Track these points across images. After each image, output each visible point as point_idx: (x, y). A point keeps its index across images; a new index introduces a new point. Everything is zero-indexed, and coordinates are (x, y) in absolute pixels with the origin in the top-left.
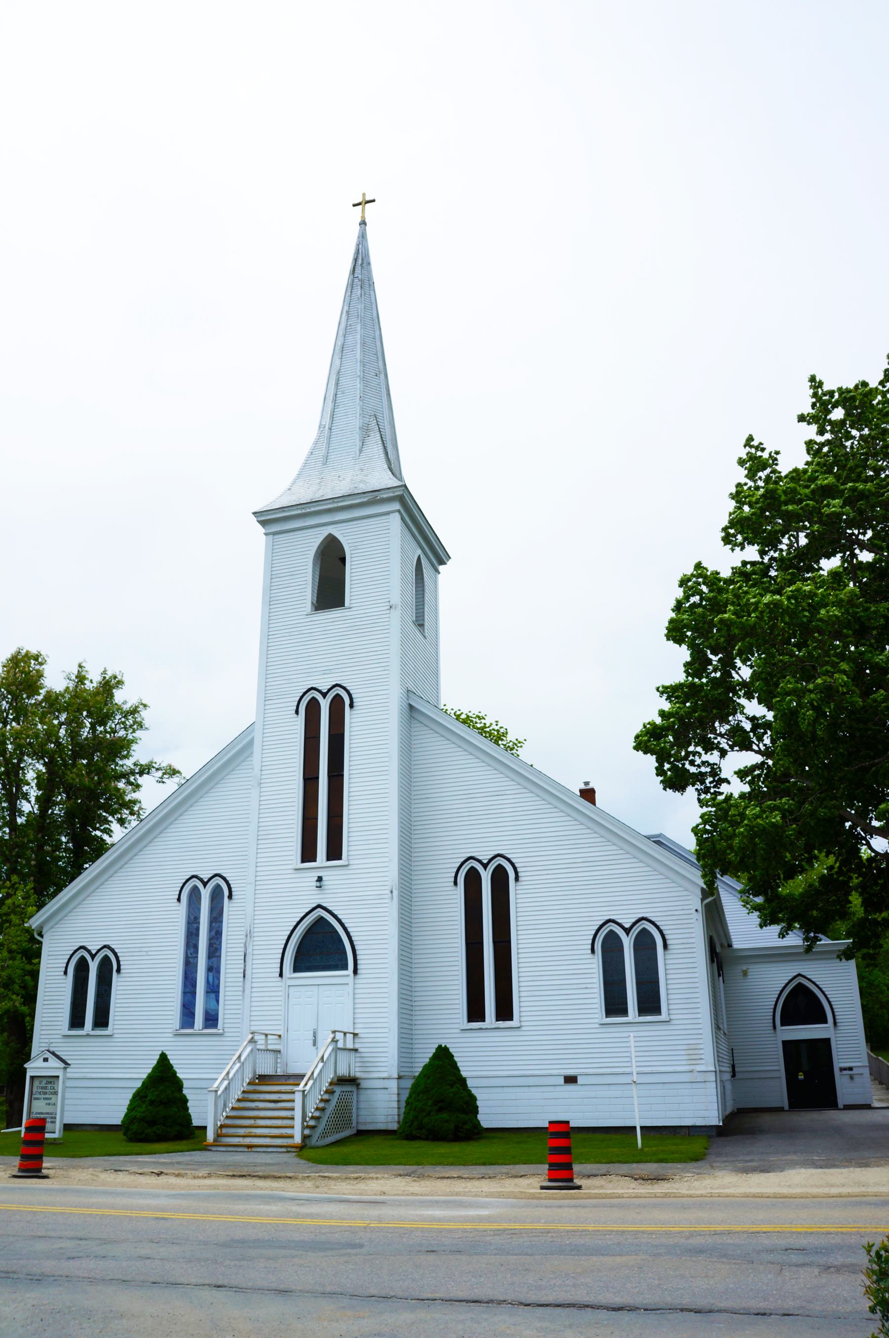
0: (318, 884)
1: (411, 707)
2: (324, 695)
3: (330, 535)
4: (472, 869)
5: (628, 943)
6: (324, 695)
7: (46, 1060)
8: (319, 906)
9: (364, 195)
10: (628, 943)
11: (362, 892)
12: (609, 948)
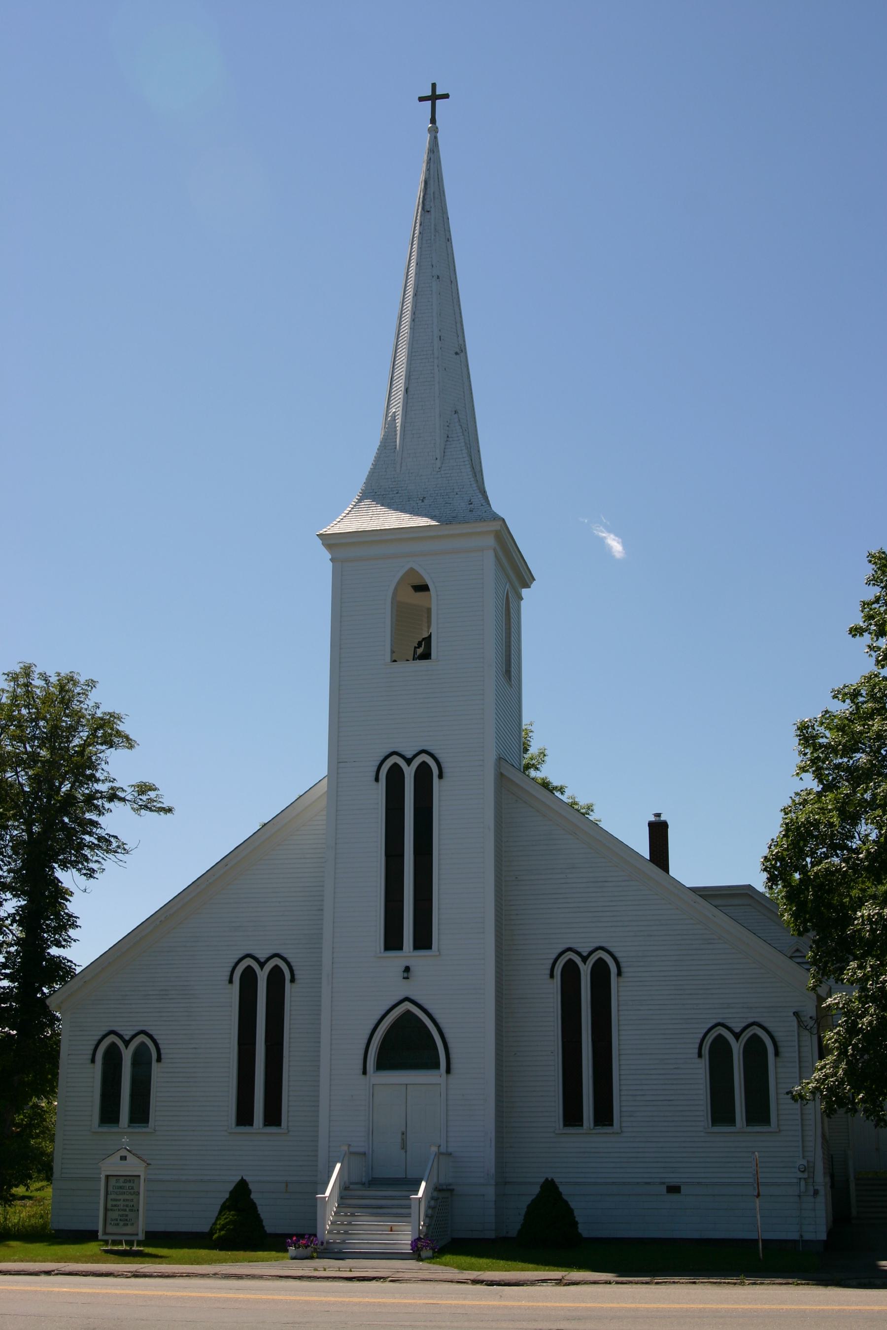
0: (406, 975)
1: (501, 774)
2: (409, 761)
3: (412, 570)
4: (571, 962)
5: (737, 1048)
6: (409, 761)
7: (123, 1158)
8: (407, 999)
9: (434, 86)
10: (737, 1048)
11: (456, 981)
12: (718, 1053)
